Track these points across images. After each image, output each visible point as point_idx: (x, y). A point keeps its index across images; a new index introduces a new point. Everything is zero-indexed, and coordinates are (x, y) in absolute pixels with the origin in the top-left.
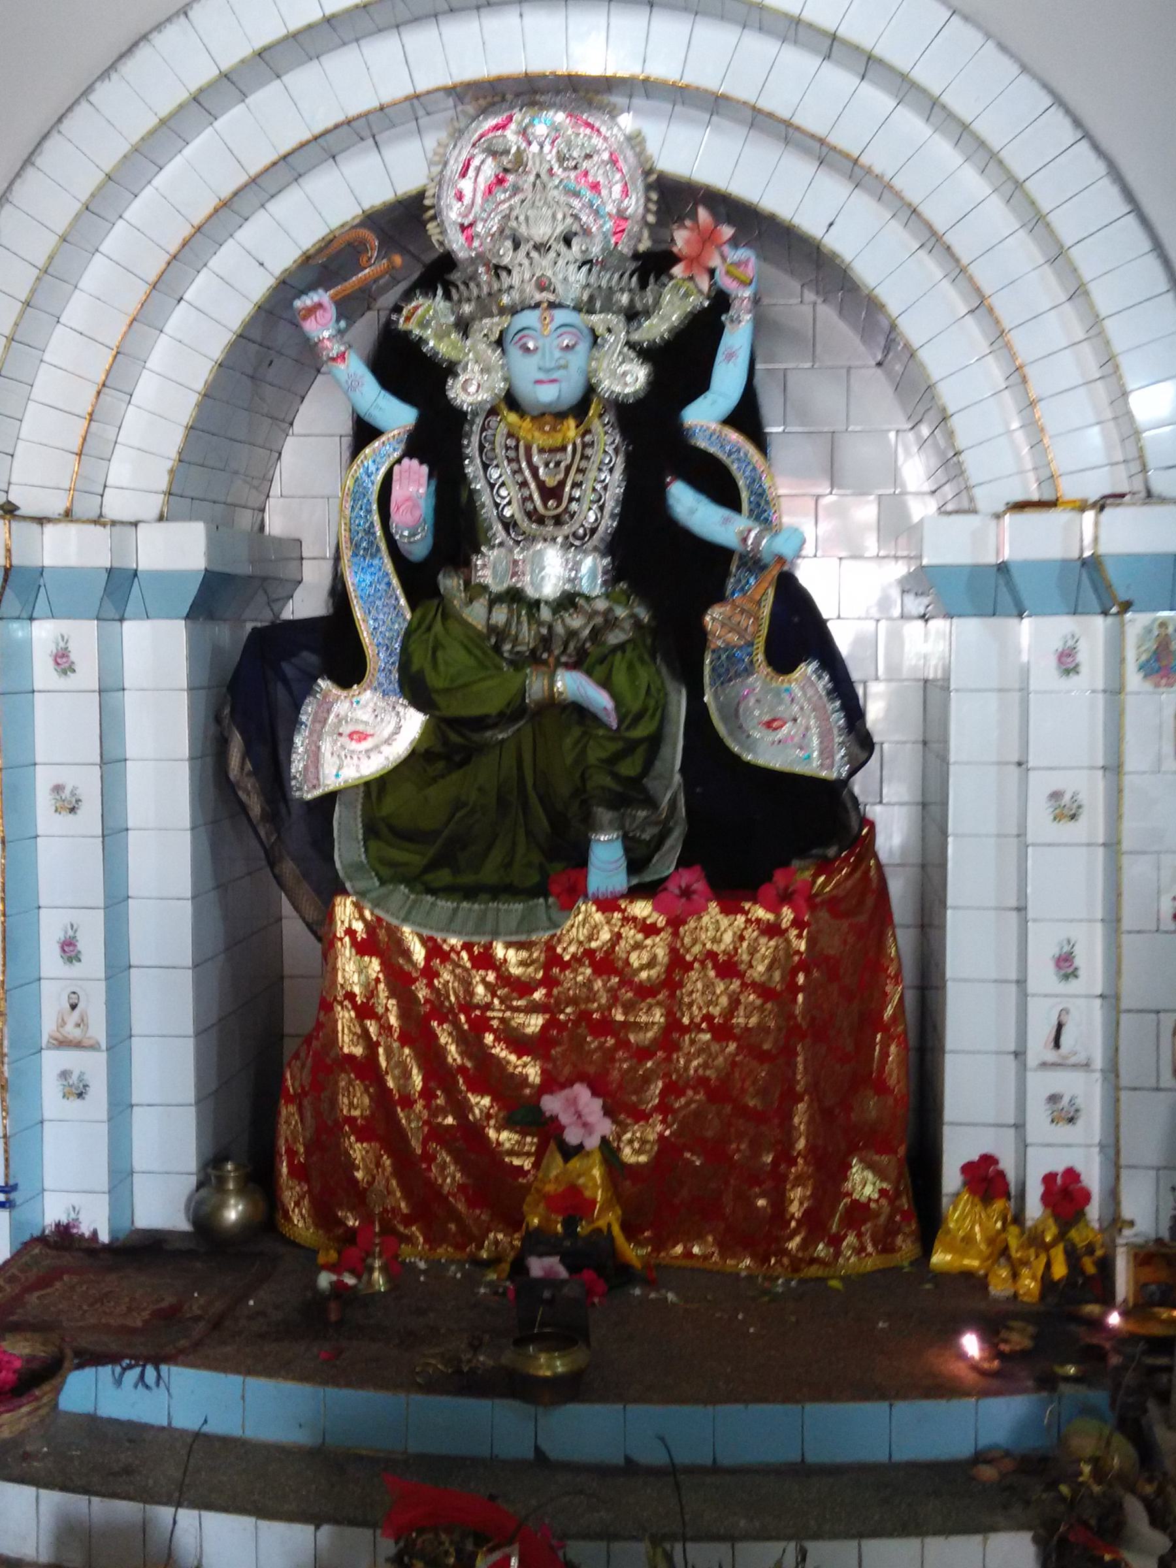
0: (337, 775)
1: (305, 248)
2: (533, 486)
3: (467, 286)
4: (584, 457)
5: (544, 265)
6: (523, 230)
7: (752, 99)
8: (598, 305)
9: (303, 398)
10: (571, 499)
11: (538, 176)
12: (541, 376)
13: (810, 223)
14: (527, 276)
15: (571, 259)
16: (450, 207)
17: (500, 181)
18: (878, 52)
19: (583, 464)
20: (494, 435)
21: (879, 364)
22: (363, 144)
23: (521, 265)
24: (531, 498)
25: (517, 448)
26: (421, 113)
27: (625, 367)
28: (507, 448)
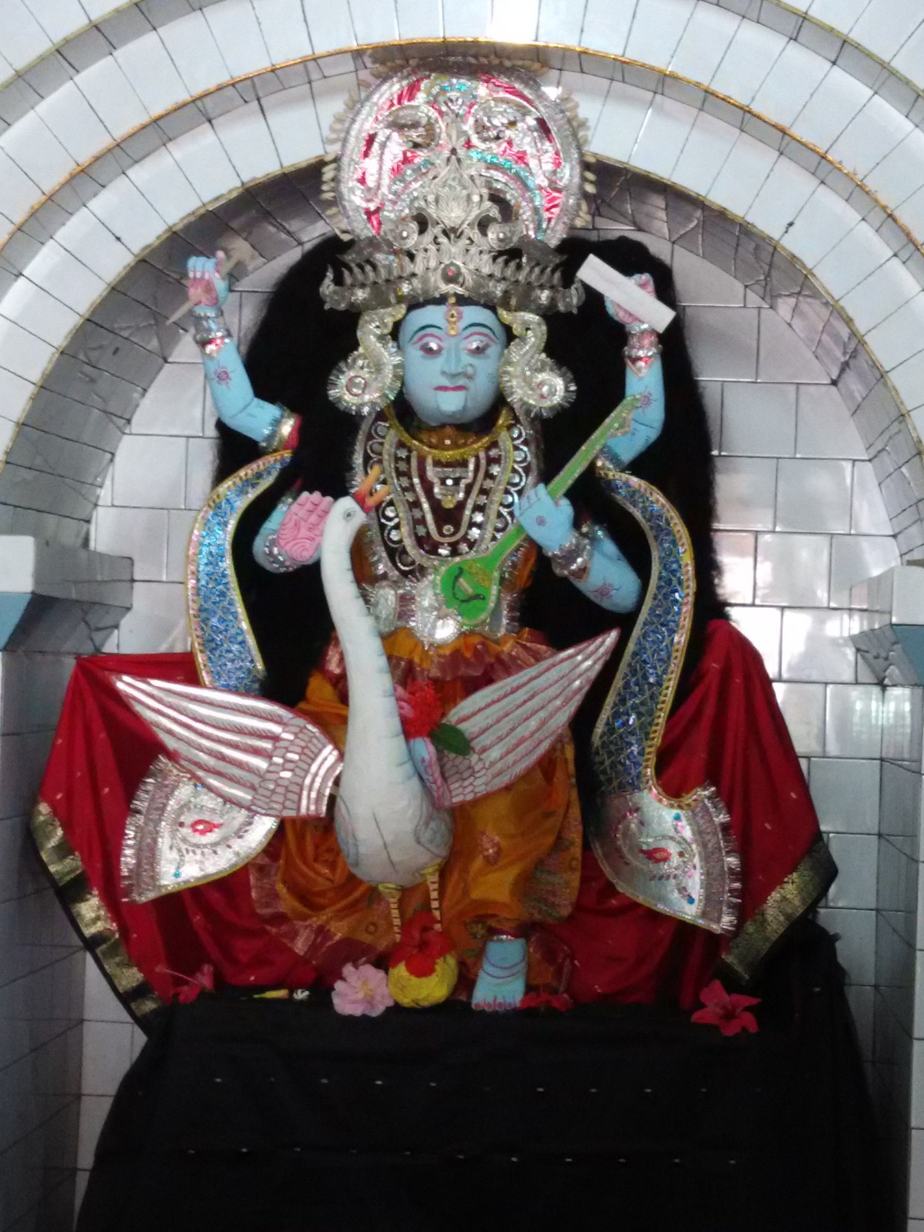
0: (177, 875)
1: (171, 223)
2: (426, 506)
3: (361, 268)
4: (489, 476)
5: (454, 252)
6: (432, 211)
7: (705, 81)
8: (513, 302)
9: (145, 390)
10: (472, 524)
11: (454, 151)
12: (445, 382)
13: (767, 221)
14: (433, 264)
15: (485, 248)
16: (352, 190)
17: (406, 160)
18: (855, 36)
19: (488, 484)
20: (382, 444)
21: (834, 383)
22: (246, 107)
23: (426, 250)
24: (423, 521)
25: (408, 460)
26: (315, 75)
27: (541, 377)
28: (397, 459)
